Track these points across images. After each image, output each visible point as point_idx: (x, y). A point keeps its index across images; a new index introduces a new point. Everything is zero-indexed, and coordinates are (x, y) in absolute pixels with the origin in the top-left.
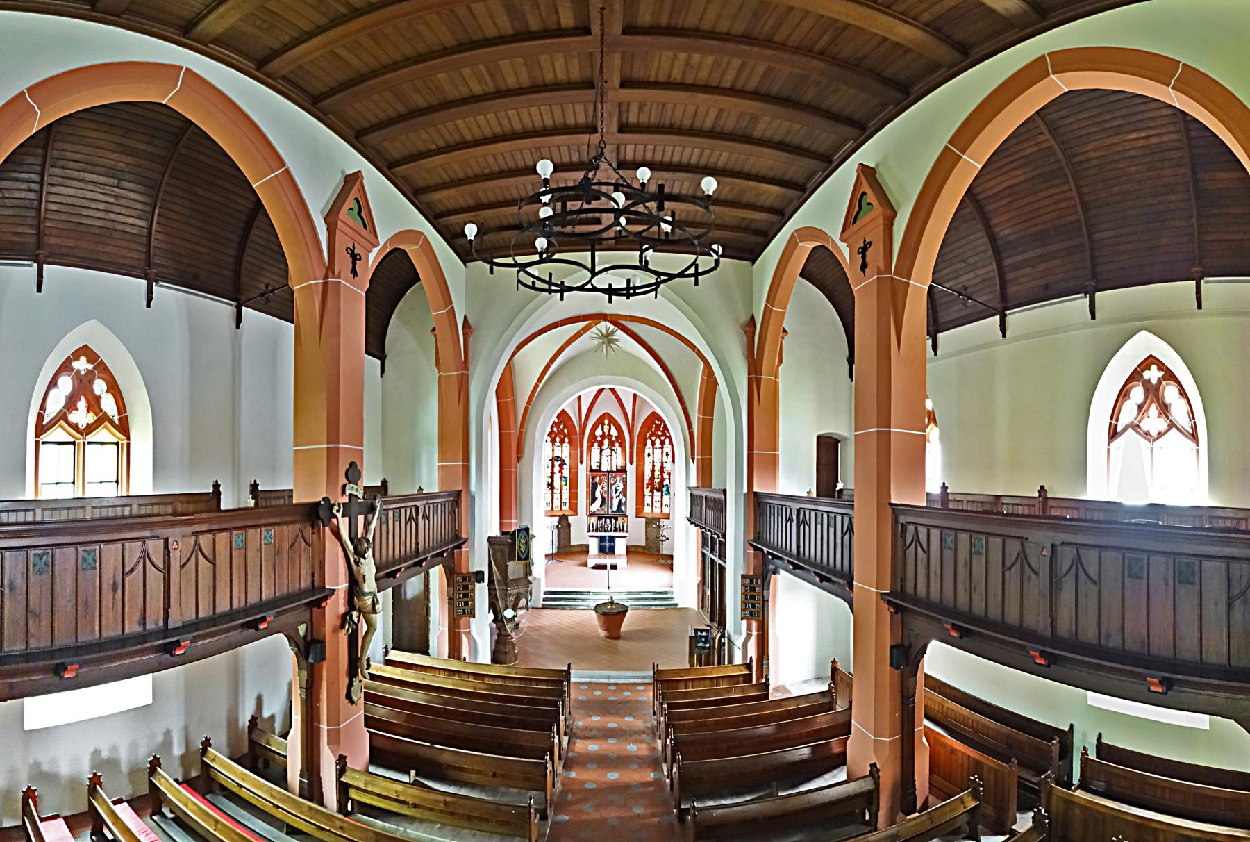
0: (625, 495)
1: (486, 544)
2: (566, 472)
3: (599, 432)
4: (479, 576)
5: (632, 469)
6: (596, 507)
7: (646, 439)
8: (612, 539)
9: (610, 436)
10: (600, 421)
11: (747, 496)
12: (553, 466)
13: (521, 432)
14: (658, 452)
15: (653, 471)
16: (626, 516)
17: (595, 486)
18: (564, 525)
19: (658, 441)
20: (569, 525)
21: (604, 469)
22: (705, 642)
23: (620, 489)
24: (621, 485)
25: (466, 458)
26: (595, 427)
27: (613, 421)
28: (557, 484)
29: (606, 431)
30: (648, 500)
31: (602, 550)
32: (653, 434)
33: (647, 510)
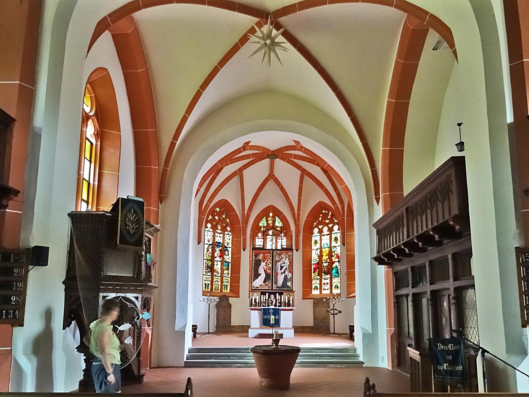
0: (291, 271)
1: (66, 224)
2: (228, 258)
3: (263, 223)
4: (40, 256)
5: (297, 256)
6: (259, 282)
7: (313, 228)
8: (276, 312)
9: (274, 228)
10: (265, 213)
11: (515, 129)
12: (214, 251)
13: (165, 172)
14: (326, 240)
15: (320, 256)
16: (292, 291)
17: (257, 264)
18: (223, 306)
19: (325, 229)
20: (230, 306)
21: (269, 247)
22: (454, 363)
23: (286, 266)
24: (287, 262)
25: (30, 75)
26: (259, 219)
27: (278, 213)
28: (218, 267)
29: (270, 222)
30: (315, 283)
31: (266, 323)
32: (320, 223)
33: (315, 292)
